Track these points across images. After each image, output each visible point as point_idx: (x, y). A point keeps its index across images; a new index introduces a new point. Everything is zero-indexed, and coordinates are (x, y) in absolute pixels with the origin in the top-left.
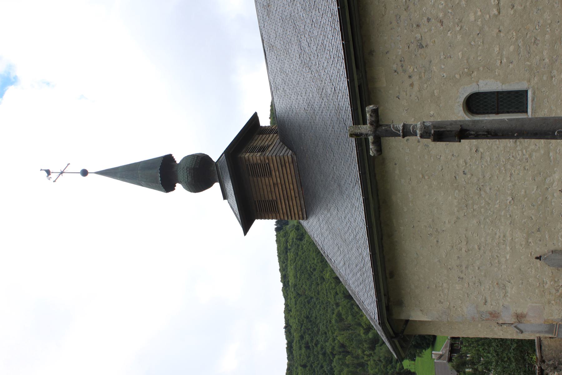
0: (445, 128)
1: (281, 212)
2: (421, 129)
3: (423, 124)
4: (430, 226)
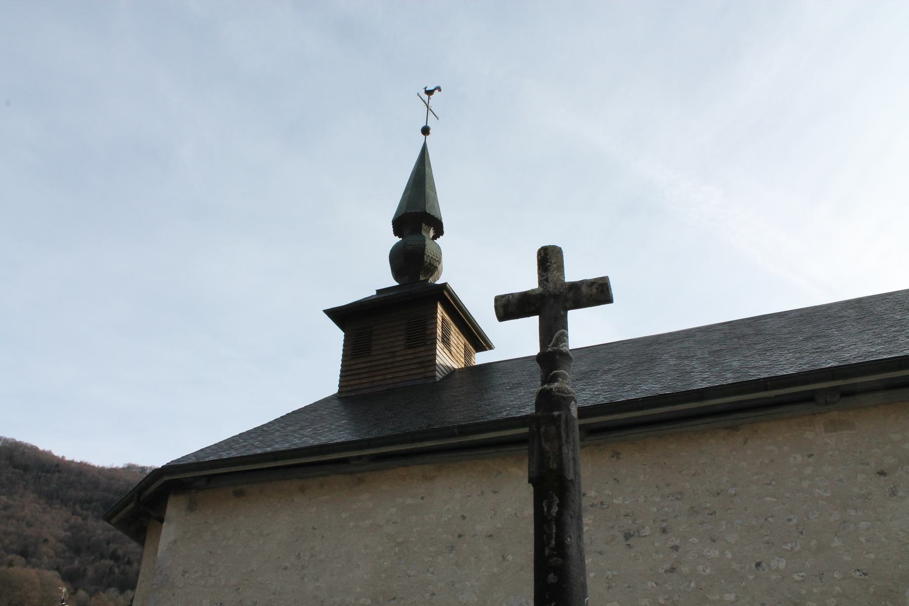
0: (567, 442)
1: (353, 362)
2: (559, 390)
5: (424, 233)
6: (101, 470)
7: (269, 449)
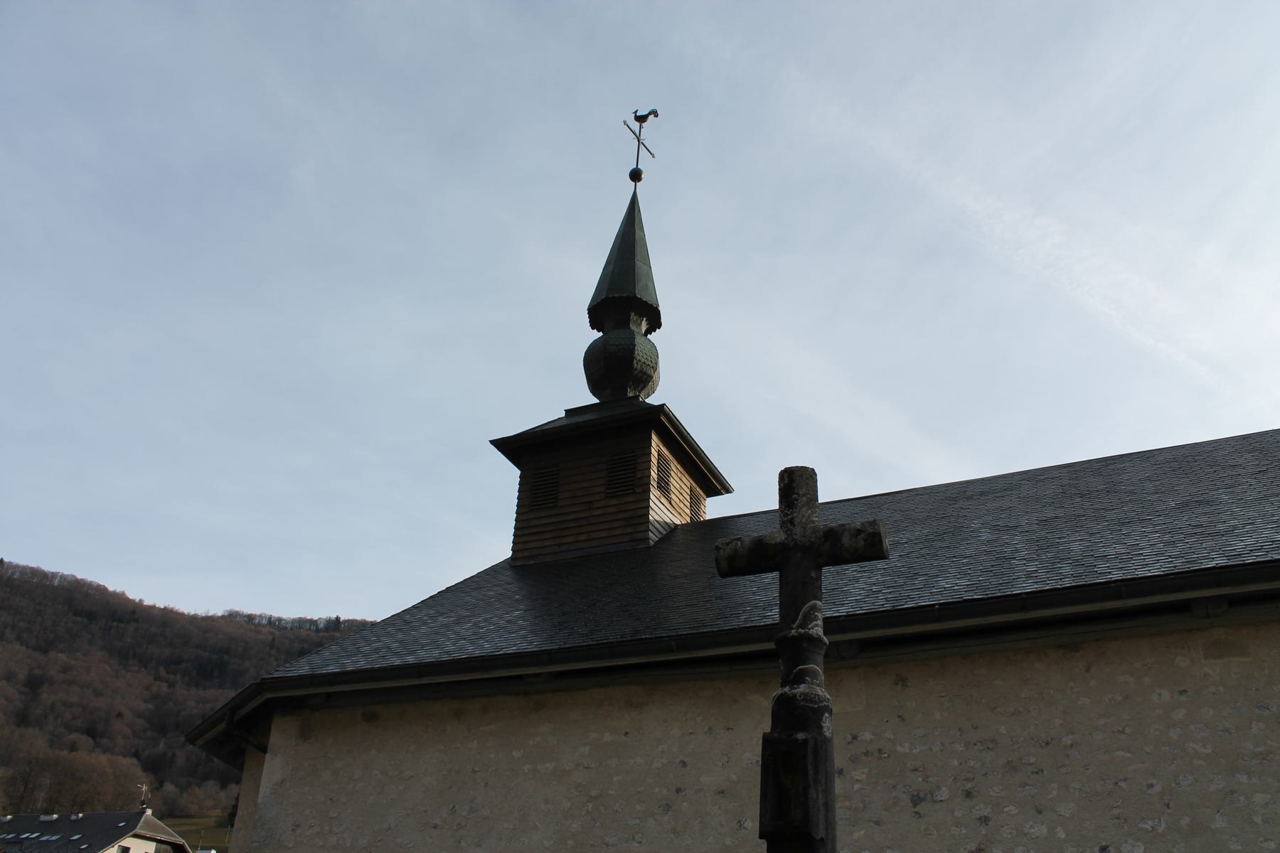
2: (805, 696)
5: (633, 327)
6: (193, 619)
7: (411, 659)
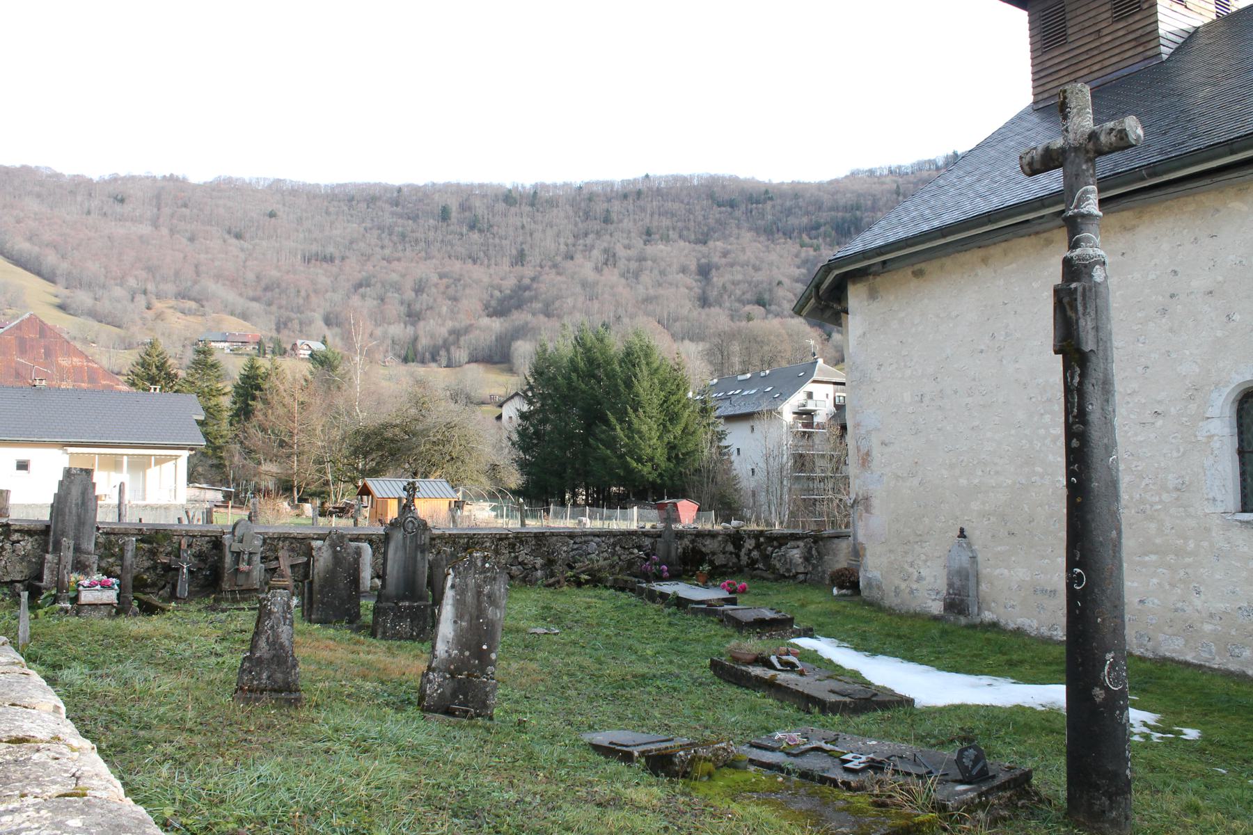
3: (1096, 263)
4: (1007, 335)
6: (820, 186)
